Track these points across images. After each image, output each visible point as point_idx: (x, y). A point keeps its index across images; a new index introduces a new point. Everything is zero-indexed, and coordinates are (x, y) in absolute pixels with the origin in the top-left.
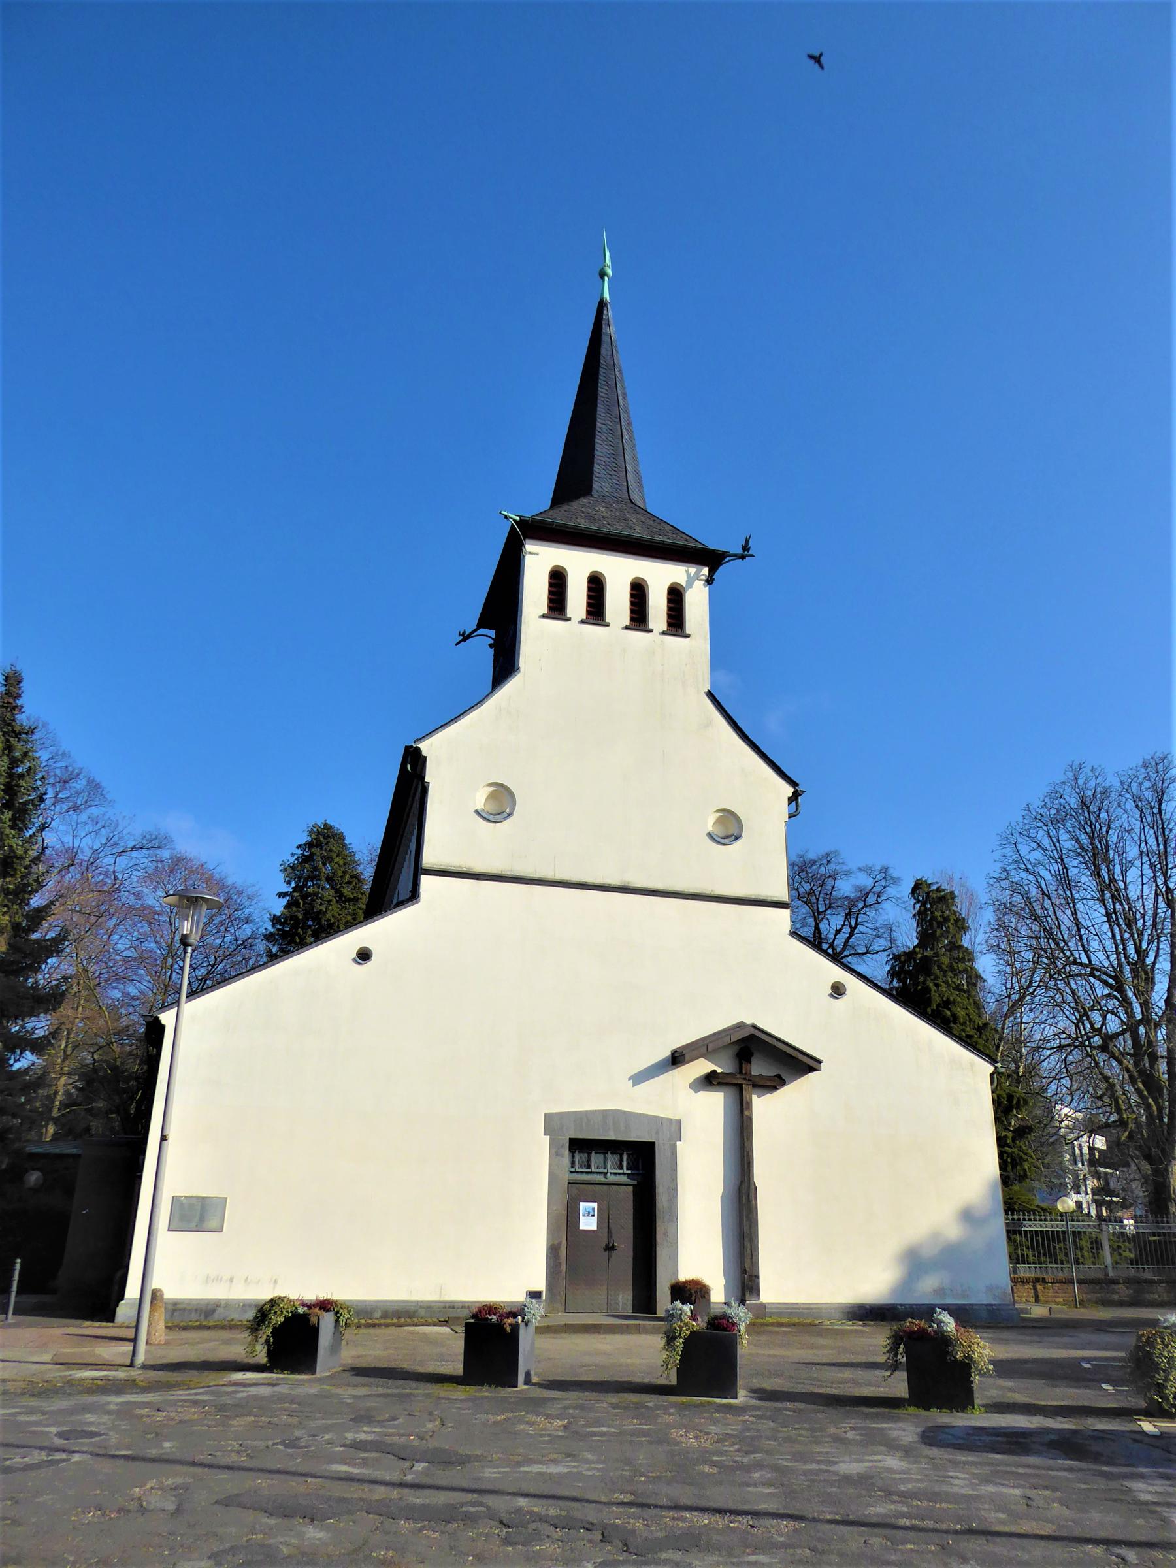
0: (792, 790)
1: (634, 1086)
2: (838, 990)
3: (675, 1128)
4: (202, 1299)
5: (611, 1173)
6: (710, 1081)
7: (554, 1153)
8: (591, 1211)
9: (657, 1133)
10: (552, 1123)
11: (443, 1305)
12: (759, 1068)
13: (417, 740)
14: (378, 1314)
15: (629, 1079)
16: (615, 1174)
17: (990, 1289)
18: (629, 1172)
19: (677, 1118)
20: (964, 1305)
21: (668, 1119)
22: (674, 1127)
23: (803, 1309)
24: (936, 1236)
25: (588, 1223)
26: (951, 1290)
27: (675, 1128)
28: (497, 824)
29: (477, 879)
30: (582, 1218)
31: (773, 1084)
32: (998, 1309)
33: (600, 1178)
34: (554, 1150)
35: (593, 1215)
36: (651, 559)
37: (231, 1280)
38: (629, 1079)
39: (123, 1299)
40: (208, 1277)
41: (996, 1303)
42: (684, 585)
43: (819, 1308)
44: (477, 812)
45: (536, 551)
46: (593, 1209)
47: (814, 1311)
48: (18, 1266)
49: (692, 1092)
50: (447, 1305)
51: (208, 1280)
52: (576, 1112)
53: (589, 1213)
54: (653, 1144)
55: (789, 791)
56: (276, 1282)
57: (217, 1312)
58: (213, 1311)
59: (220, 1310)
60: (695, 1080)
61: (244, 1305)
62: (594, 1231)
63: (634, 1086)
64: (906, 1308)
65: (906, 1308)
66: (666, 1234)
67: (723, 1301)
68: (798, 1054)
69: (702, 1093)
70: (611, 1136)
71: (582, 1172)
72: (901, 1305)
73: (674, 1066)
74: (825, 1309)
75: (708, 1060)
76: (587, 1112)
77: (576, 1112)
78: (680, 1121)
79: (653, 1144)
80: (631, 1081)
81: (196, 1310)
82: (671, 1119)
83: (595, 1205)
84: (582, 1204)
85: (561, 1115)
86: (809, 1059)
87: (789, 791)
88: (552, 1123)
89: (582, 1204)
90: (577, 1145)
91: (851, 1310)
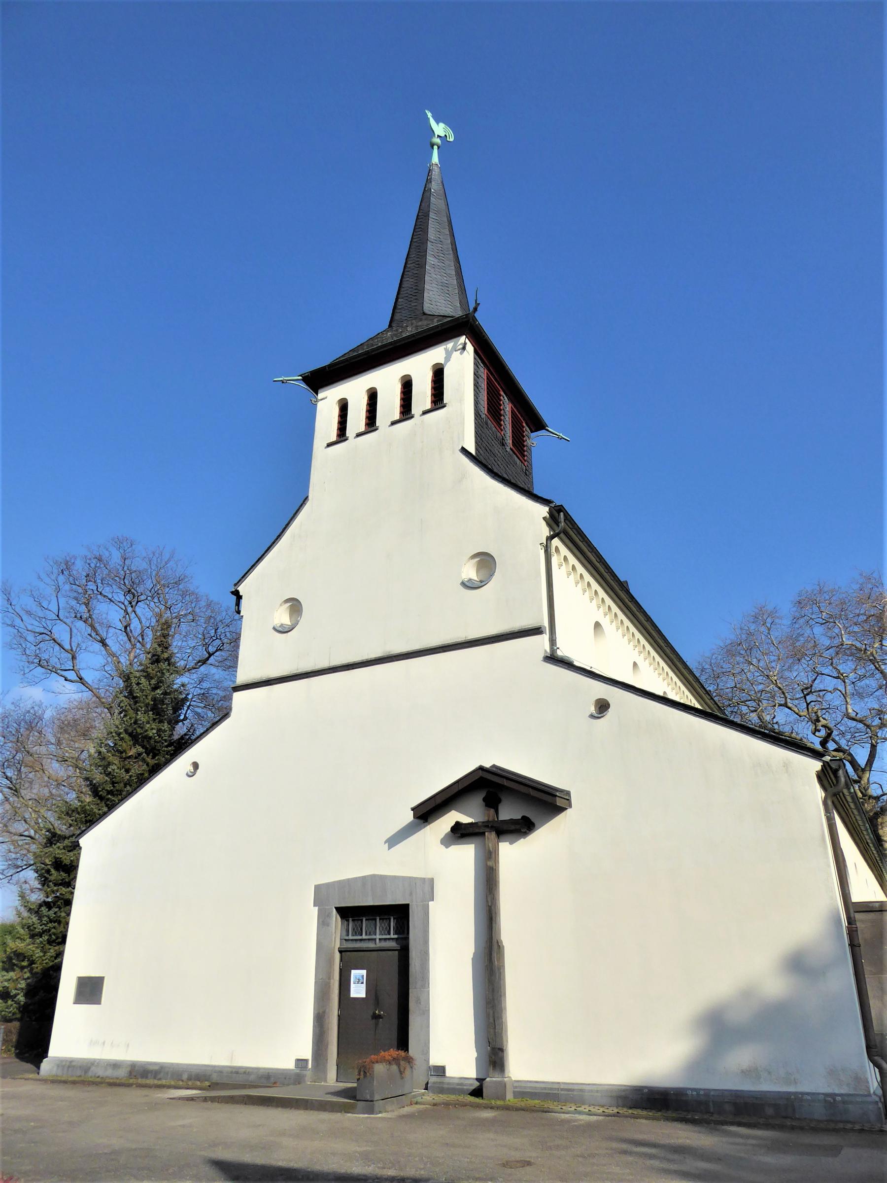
0: (547, 509)
1: (389, 848)
2: (603, 707)
3: (427, 887)
4: (138, 1061)
5: (380, 939)
6: (460, 833)
7: (323, 922)
8: (361, 978)
9: (411, 894)
10: (321, 894)
11: (230, 1070)
12: (508, 812)
13: (235, 585)
14: (185, 1077)
15: (385, 843)
16: (385, 939)
17: (832, 1072)
18: (396, 936)
19: (430, 877)
20: (790, 1093)
21: (421, 879)
22: (427, 888)
23: (562, 1090)
24: (747, 994)
25: (358, 991)
26: (769, 1073)
27: (427, 887)
28: (289, 633)
29: (270, 685)
30: (352, 986)
31: (524, 827)
32: (844, 1102)
33: (371, 945)
34: (321, 920)
35: (362, 983)
36: (410, 356)
37: (104, 1043)
38: (385, 844)
39: (47, 1057)
40: (91, 1041)
41: (842, 1092)
42: (443, 363)
43: (581, 1090)
44: (274, 629)
45: (324, 396)
46: (363, 976)
47: (575, 1093)
48: (429, 115)
49: (443, 847)
50: (234, 1070)
51: (92, 1043)
52: (340, 882)
53: (359, 981)
54: (408, 905)
55: (544, 510)
56: (128, 1045)
57: (92, 1069)
58: (89, 1068)
59: (93, 1068)
60: (446, 834)
61: (107, 1065)
62: (362, 998)
63: (389, 848)
64: (698, 1094)
65: (698, 1094)
66: (418, 1001)
67: (475, 1077)
68: (531, 790)
69: (453, 847)
70: (370, 902)
71: (356, 940)
72: (693, 1090)
73: (425, 824)
74: (592, 1091)
75: (457, 811)
76: (348, 880)
77: (340, 881)
78: (432, 881)
79: (408, 905)
80: (387, 844)
81: (80, 1067)
82: (424, 879)
83: (364, 972)
84: (353, 971)
85: (328, 885)
86: (539, 793)
87: (544, 510)
88: (321, 894)
89: (353, 971)
90: (345, 913)
91: (623, 1094)
